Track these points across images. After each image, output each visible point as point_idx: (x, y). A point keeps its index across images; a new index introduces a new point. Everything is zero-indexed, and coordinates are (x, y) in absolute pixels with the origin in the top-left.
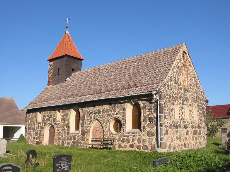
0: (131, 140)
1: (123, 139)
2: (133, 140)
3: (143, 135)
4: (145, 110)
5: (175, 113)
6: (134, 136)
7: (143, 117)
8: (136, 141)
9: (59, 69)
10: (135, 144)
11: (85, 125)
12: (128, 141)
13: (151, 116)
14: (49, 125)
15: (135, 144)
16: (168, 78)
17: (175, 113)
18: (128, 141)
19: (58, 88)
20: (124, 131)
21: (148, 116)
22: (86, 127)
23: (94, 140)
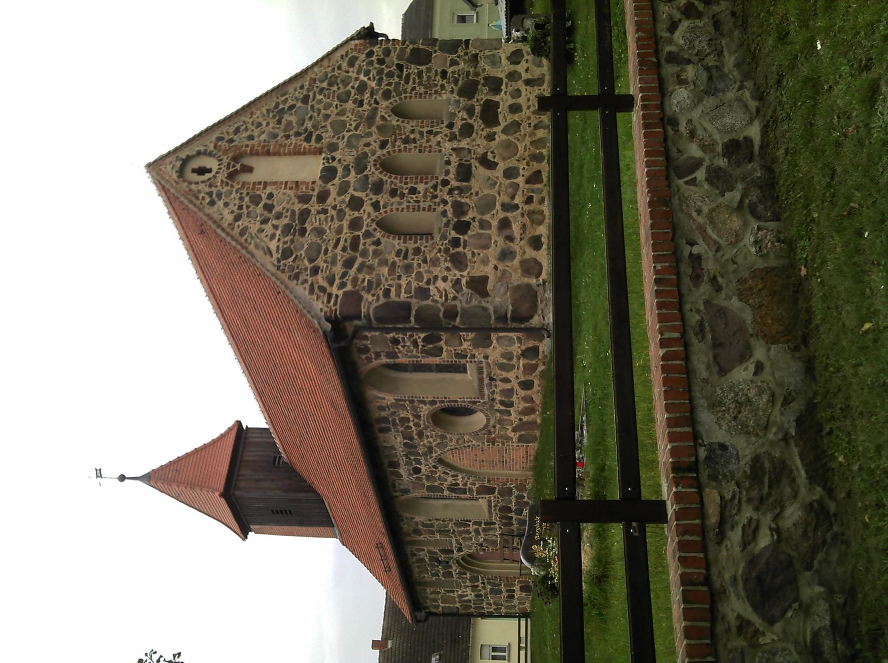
0: (508, 386)
1: (502, 403)
2: (506, 380)
3: (486, 357)
4: (400, 352)
5: (424, 209)
6: (491, 379)
7: (423, 357)
8: (511, 375)
9: (122, 478)
10: (517, 377)
11: (461, 486)
12: (509, 393)
13: (419, 340)
14: (485, 567)
15: (517, 377)
16: (283, 271)
17: (424, 209)
18: (509, 393)
19: (186, 202)
20: (475, 403)
21: (420, 347)
22: (465, 484)
23: (463, 496)
